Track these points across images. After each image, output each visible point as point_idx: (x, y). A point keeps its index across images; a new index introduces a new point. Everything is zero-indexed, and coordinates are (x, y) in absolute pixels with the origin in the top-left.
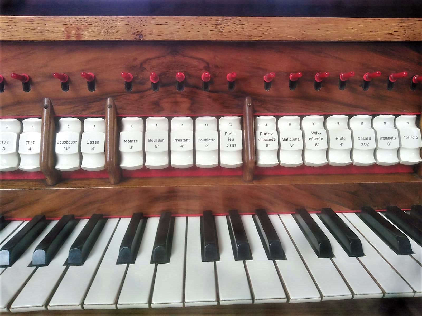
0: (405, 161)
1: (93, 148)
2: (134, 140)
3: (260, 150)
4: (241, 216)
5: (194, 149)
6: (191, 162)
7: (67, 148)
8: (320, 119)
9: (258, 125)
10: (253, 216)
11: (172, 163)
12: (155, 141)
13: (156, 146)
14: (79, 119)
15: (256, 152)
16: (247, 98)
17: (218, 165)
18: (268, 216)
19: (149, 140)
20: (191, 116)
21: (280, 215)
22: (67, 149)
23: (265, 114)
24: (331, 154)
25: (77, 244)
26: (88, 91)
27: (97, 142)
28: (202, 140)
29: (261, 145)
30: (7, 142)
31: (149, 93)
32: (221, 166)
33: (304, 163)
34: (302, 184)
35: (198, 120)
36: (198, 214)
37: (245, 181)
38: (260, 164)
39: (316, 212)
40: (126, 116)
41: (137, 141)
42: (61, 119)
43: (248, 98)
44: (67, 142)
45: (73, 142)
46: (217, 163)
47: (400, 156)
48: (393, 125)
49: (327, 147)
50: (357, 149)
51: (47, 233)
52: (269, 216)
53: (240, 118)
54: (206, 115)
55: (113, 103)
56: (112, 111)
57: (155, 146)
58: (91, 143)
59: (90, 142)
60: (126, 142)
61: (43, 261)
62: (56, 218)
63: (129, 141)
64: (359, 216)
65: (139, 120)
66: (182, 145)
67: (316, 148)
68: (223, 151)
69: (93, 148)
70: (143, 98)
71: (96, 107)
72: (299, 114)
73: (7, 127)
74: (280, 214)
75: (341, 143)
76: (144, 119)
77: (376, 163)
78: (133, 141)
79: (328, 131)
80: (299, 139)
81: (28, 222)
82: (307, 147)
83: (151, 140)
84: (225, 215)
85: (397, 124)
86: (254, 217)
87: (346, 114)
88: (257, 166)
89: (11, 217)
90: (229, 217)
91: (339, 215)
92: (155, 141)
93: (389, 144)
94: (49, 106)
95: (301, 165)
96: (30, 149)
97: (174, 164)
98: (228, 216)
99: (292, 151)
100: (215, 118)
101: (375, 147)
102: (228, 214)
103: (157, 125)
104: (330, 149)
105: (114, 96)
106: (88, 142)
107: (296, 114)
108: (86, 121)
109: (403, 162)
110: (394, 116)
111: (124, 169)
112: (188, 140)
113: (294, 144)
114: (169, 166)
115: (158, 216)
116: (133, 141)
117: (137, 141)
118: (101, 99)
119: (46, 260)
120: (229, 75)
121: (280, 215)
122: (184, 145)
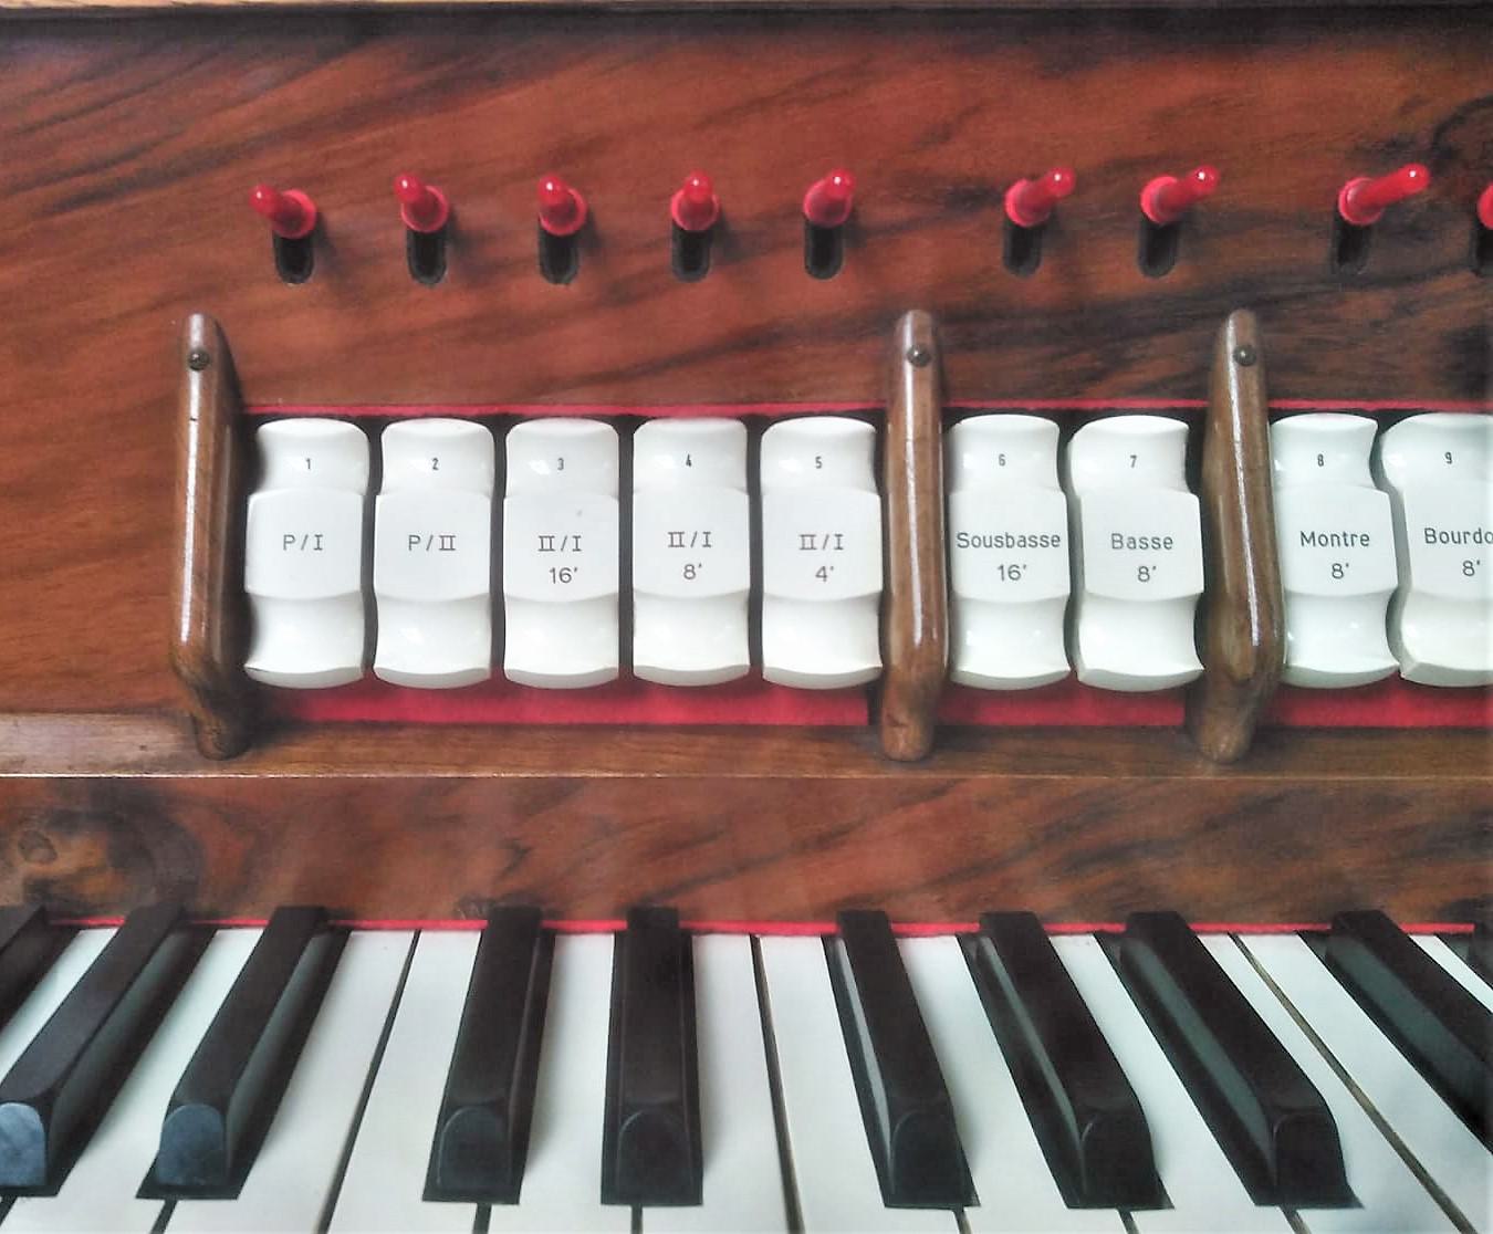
0: (654, 668)
1: (1340, 570)
2: (1349, 534)
3: (1301, 595)
4: (694, 938)
5: (363, 587)
6: (739, 657)
7: (1012, 572)
8: (1361, 430)
9: (1276, 462)
10: (828, 941)
11: (382, 663)
12: (1458, 539)
13: (687, 571)
14: (358, 429)
15: (946, 607)
16: (1232, 316)
17: (747, 671)
18: (895, 944)
19: (1427, 535)
20: (350, 413)
21: (1245, 939)
22: (1015, 575)
23: (554, 410)
24: (1090, 629)
25: (206, 1078)
26: (1139, 274)
27: (1162, 543)
28: (982, 542)
29: (974, 573)
30: (701, 539)
31: (1442, 285)
32: (764, 677)
33: (1074, 672)
34: (1047, 777)
35: (780, 436)
36: (738, 921)
37: (887, 760)
38: (967, 672)
39: (1090, 927)
40: (1306, 404)
41: (1365, 540)
42: (964, 422)
43: (915, 315)
44: (1010, 540)
45: (1038, 541)
46: (747, 662)
47: (1400, 633)
48: (1368, 470)
49: (1068, 591)
50: (1431, 599)
51: (53, 1010)
52: (899, 944)
53: (1184, 426)
54: (455, 412)
55: (216, 345)
56: (215, 381)
57: (1332, 570)
58: (1132, 545)
59: (1125, 541)
60: (1308, 542)
61: (36, 1156)
62: (917, 927)
63: (1323, 540)
64: (1323, 955)
65: (470, 438)
66: (824, 568)
67: (561, 592)
68: (775, 599)
69: (1340, 570)
70: (1410, 314)
71: (1160, 357)
72: (1371, 407)
73: (689, 463)
74: (1241, 933)
75: (824, 568)
76: (373, 427)
77: (1396, 675)
78: (1346, 539)
79: (1078, 502)
80: (1050, 541)
81: (1422, 938)
82: (1091, 583)
83: (1437, 536)
84: (607, 932)
85: (1392, 459)
86: (831, 949)
87: (598, 415)
88: (956, 685)
89: (351, 915)
90: (841, 946)
91: (1220, 948)
92: (1332, 536)
93: (1338, 570)
94: (216, 356)
95: (740, 674)
96: (822, 574)
97: (384, 666)
98: (834, 942)
99: (575, 604)
100: (610, 427)
101: (1393, 583)
102: (831, 928)
103: (1449, 456)
104: (1086, 597)
105: (1263, 303)
106: (1117, 541)
107: (1031, 406)
108: (519, 435)
109: (1415, 670)
110: (1371, 424)
111: (274, 687)
112: (1342, 539)
113: (704, 566)
114: (365, 675)
115: (607, 925)
116: (1346, 539)
117: (1365, 540)
118: (1204, 313)
119: (47, 1158)
120: (812, 193)
121: (1245, 939)
122: (832, 568)
